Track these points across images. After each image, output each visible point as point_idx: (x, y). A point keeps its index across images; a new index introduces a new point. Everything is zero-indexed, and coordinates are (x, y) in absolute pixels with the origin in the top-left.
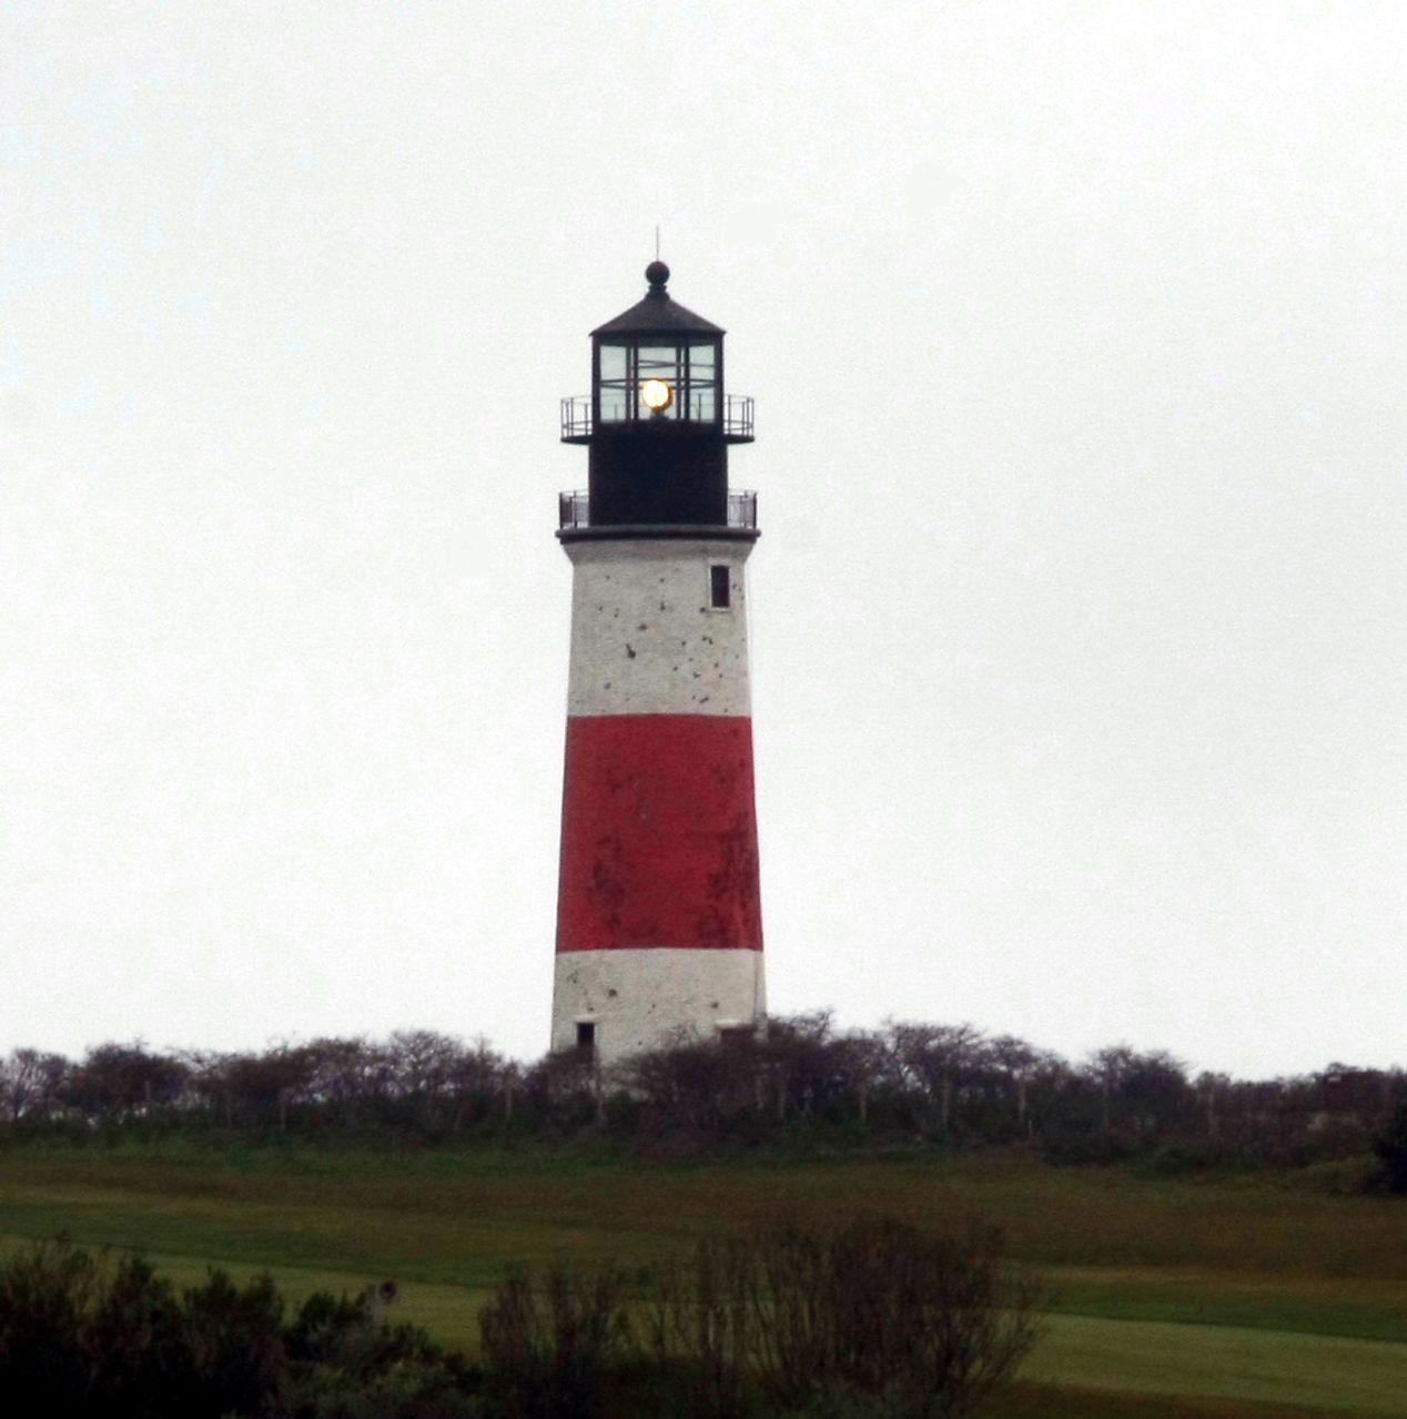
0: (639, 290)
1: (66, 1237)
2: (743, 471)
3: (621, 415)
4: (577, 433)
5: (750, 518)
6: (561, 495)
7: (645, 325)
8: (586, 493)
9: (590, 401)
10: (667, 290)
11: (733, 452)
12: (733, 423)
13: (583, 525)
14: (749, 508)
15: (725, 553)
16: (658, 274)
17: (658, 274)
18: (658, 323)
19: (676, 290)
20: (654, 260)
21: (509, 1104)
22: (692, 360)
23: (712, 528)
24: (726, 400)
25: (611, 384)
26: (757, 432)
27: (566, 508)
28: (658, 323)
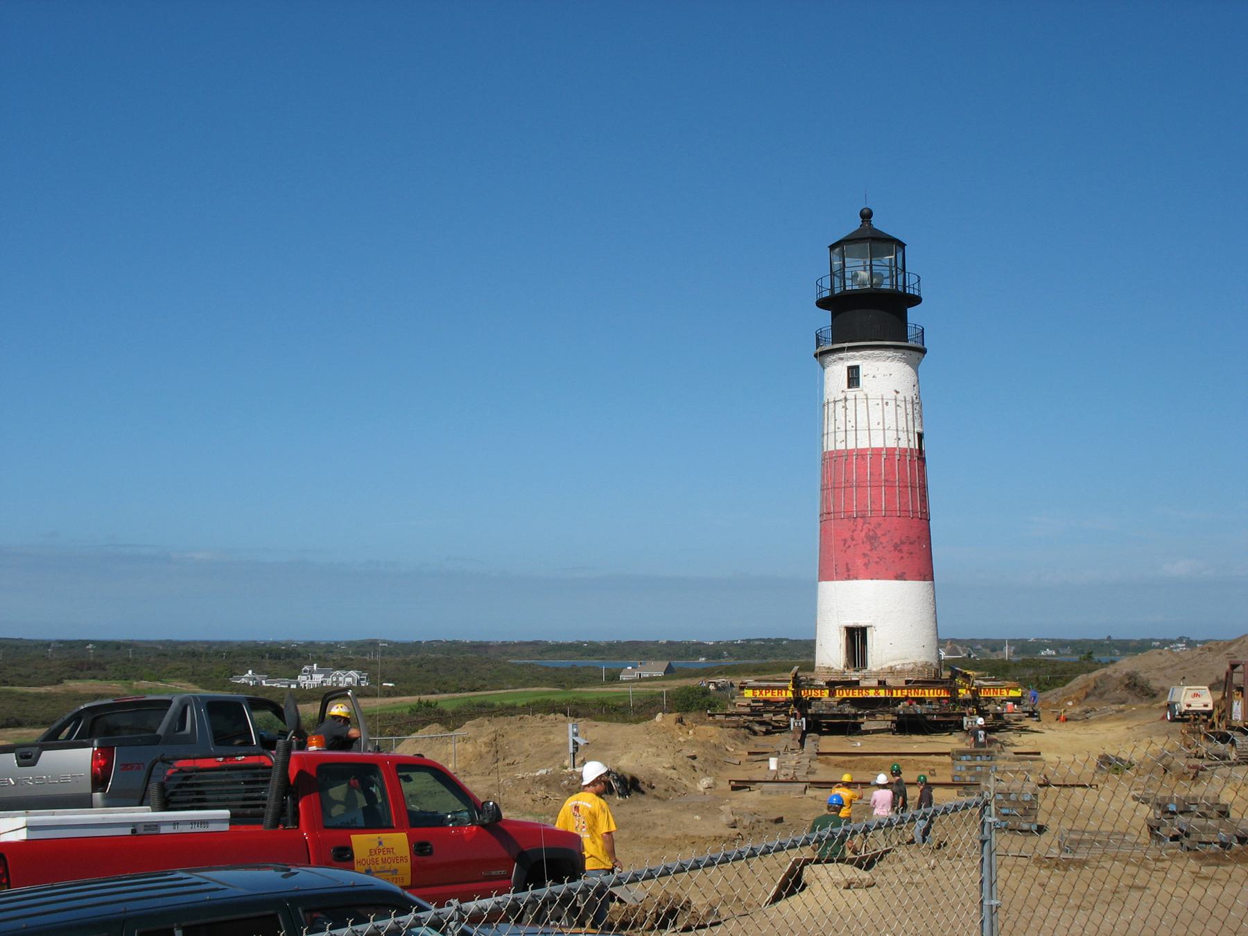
13: (829, 347)
16: (866, 216)
17: (866, 216)
28: (871, 239)
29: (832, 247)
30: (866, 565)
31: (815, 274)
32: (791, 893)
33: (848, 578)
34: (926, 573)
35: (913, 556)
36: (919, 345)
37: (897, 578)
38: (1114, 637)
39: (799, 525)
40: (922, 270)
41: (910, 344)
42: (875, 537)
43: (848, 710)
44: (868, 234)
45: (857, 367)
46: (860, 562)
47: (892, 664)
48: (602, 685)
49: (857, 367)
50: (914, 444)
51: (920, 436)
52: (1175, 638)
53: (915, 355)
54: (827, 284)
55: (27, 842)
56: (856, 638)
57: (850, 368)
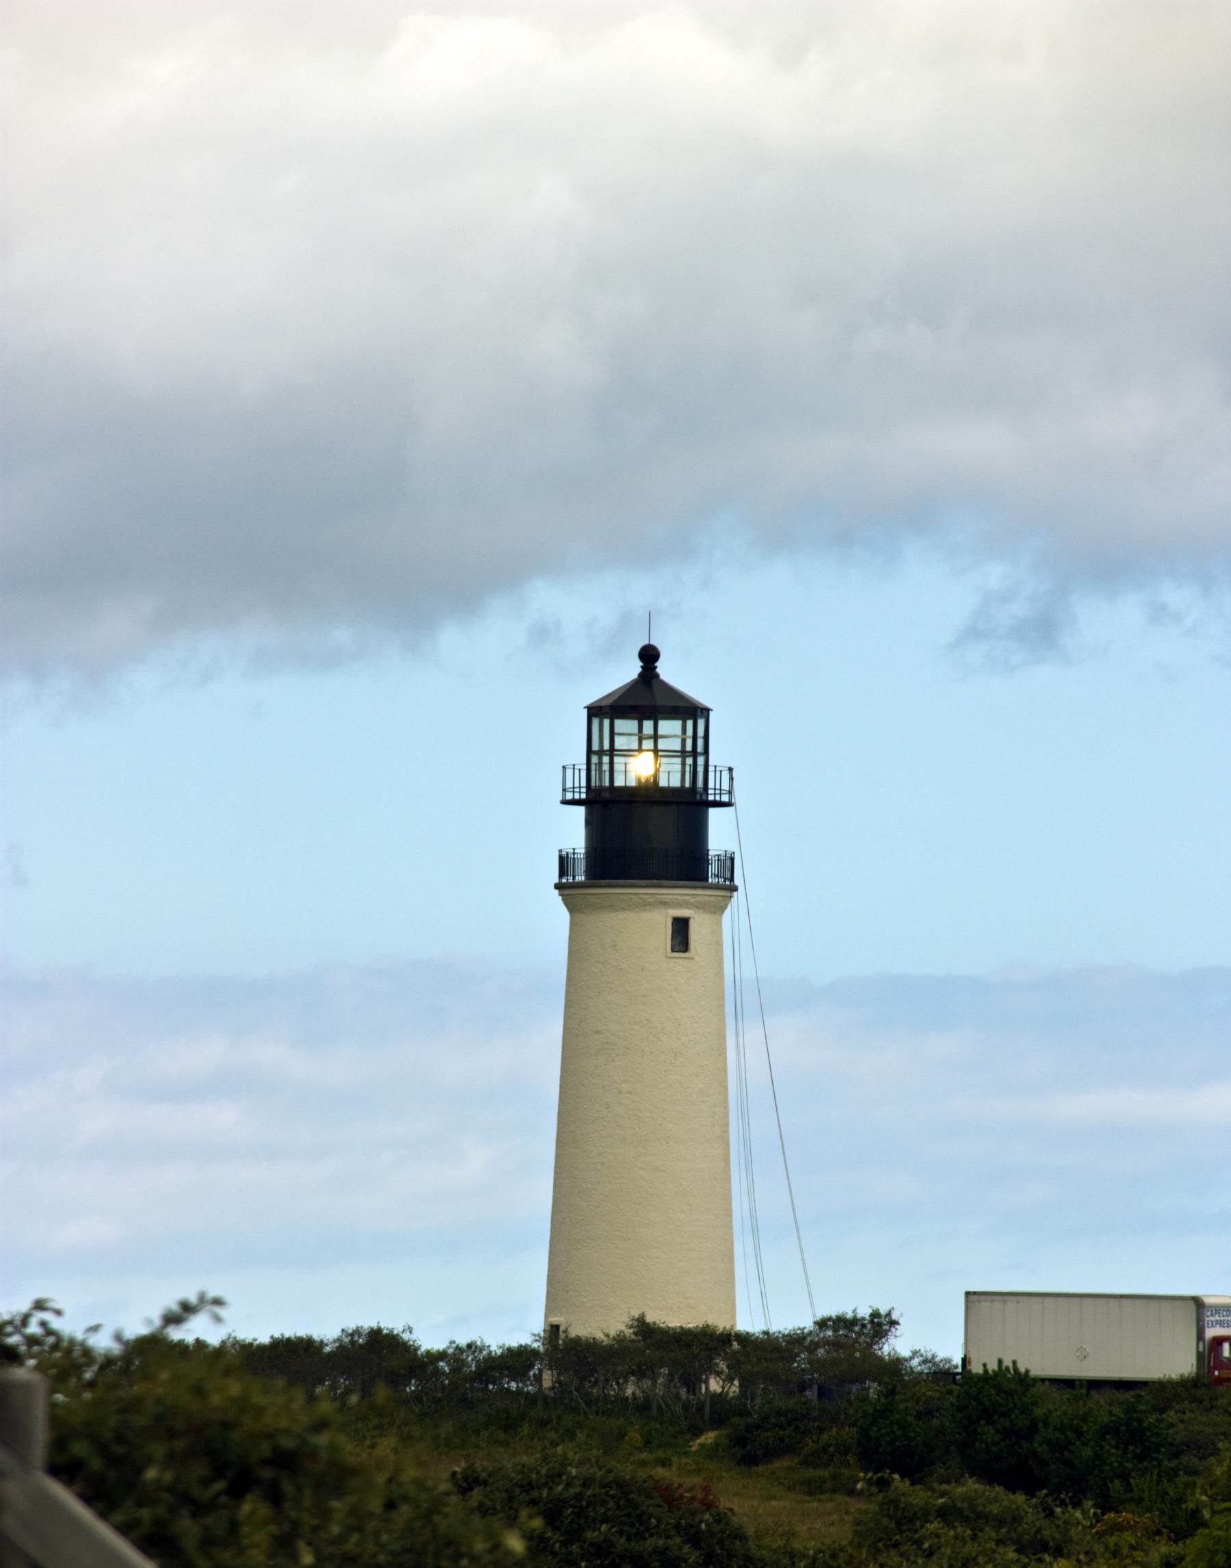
0: (632, 670)
1: (592, 1550)
2: (720, 832)
3: (675, 782)
4: (577, 796)
5: (728, 875)
6: (560, 851)
7: (630, 703)
8: (583, 851)
9: (584, 767)
10: (658, 670)
11: (713, 813)
12: (717, 784)
14: (729, 863)
15: (686, 905)
16: (649, 655)
17: (649, 655)
18: (647, 698)
19: (666, 670)
20: (646, 642)
21: (708, 1406)
22: (617, 730)
23: (704, 884)
24: (711, 769)
25: (649, 737)
26: (738, 797)
27: (564, 863)
28: (647, 698)
29: (595, 711)
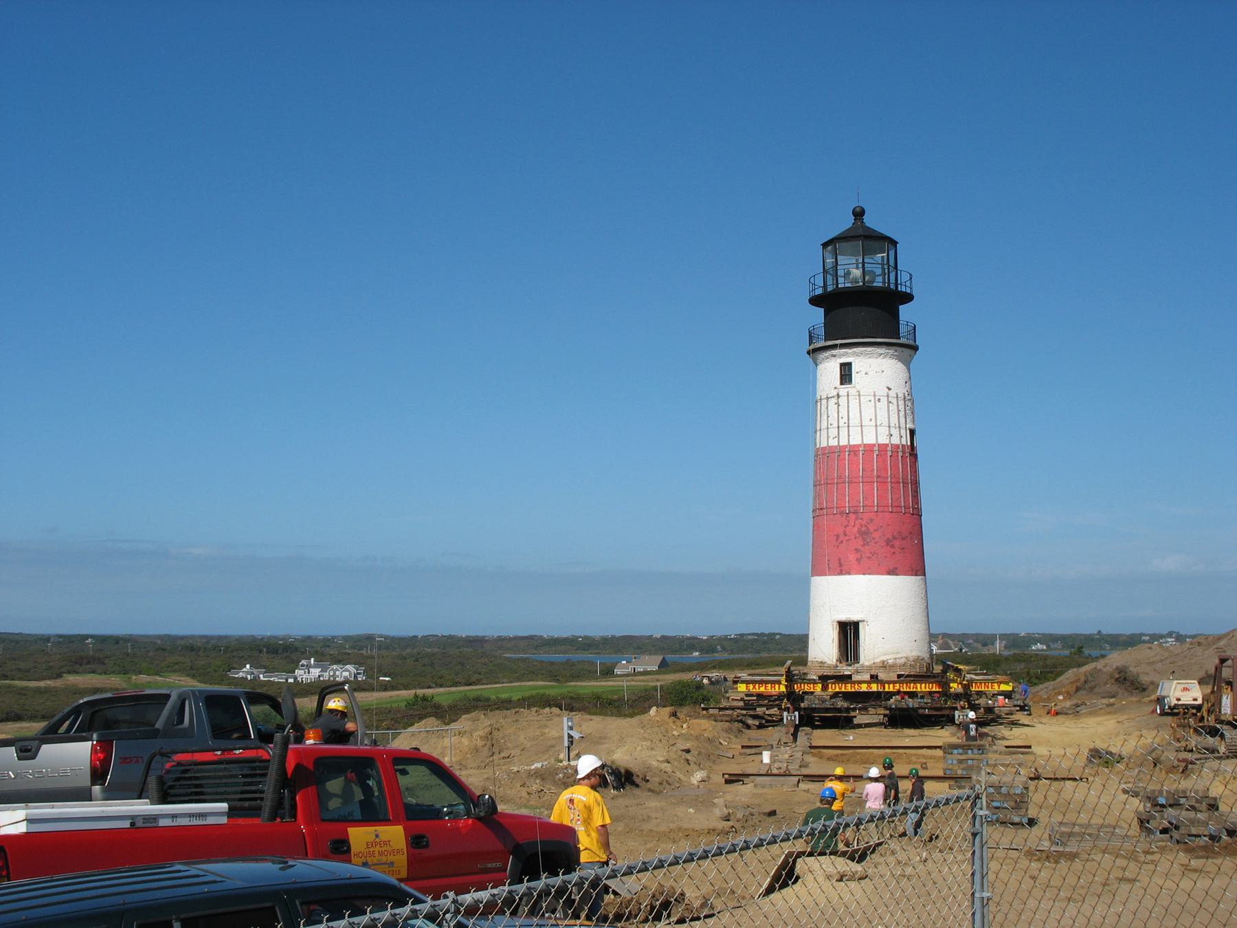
13: (822, 344)
16: (859, 214)
17: (859, 214)
28: (863, 237)
29: (825, 245)
30: (858, 560)
31: (808, 272)
32: (784, 885)
33: (841, 573)
34: (918, 569)
35: (905, 552)
36: (911, 342)
37: (889, 573)
38: (1104, 632)
39: (792, 521)
40: (913, 268)
41: (902, 341)
42: (867, 533)
43: (841, 704)
44: (861, 232)
45: (850, 364)
46: (852, 557)
47: (884, 658)
48: (597, 679)
49: (850, 364)
50: (906, 441)
51: (912, 432)
52: (1165, 633)
53: (907, 352)
54: (819, 281)
55: (27, 835)
56: (849, 632)
57: (842, 365)
